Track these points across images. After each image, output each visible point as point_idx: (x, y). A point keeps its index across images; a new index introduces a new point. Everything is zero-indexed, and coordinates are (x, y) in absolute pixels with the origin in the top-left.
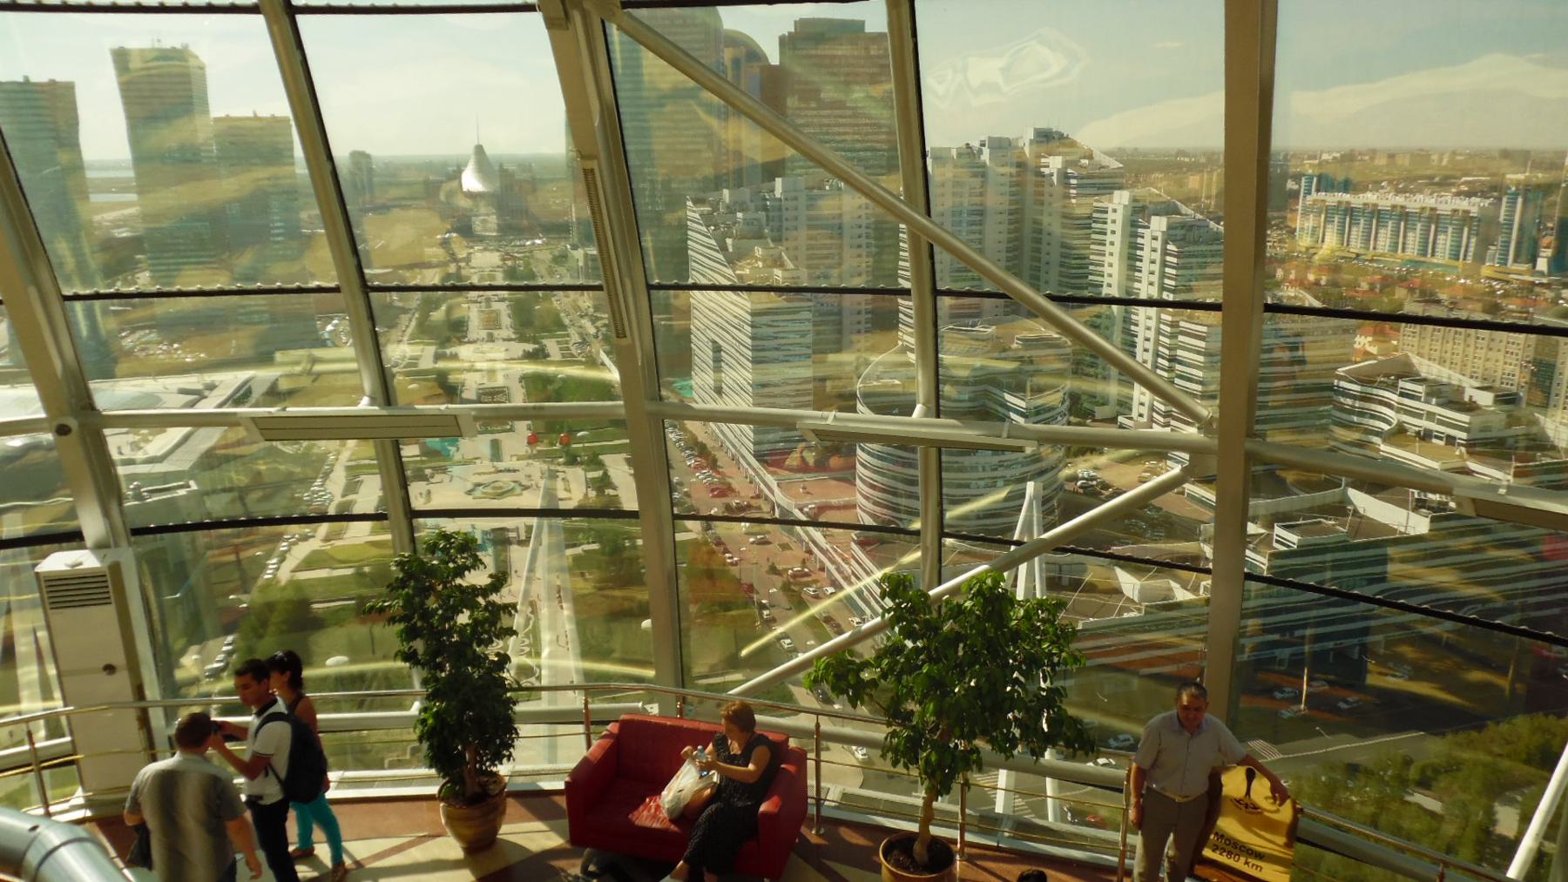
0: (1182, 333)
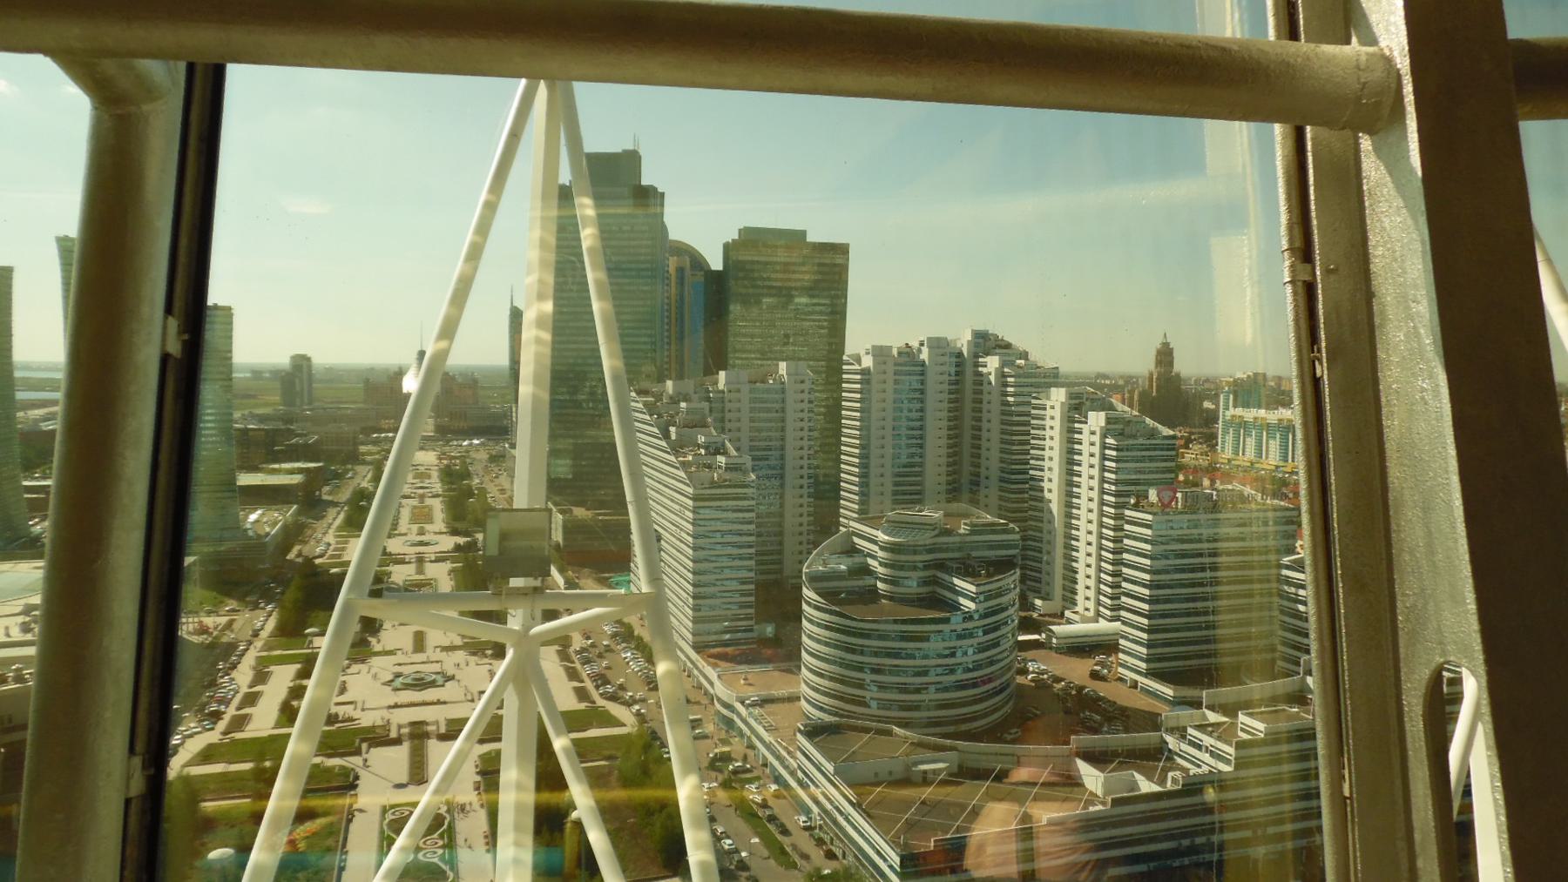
0: (1128, 537)
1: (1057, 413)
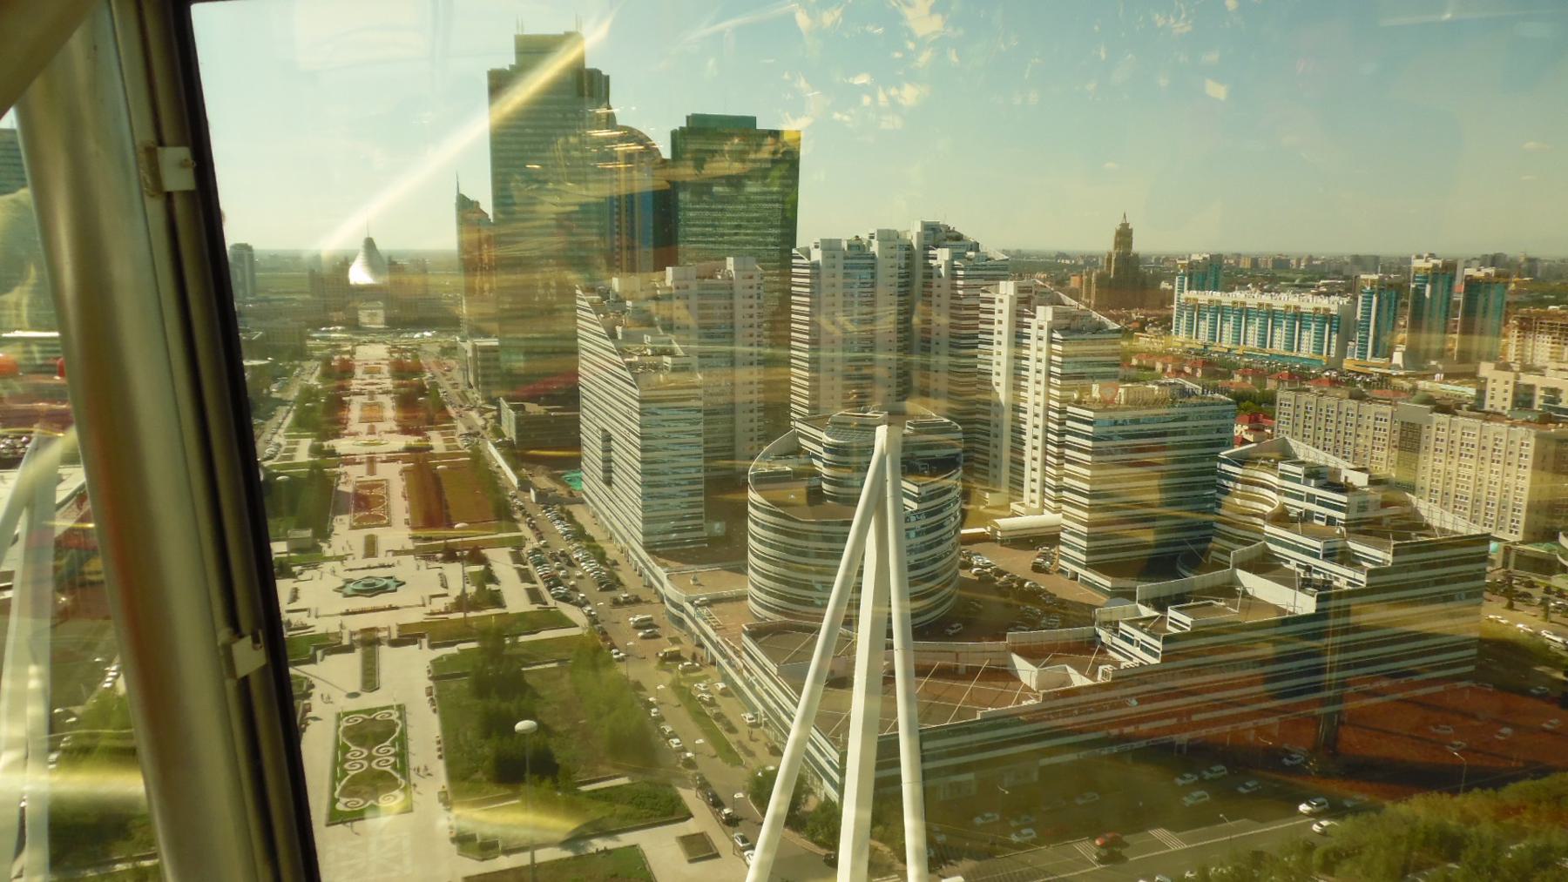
1: (1006, 307)
